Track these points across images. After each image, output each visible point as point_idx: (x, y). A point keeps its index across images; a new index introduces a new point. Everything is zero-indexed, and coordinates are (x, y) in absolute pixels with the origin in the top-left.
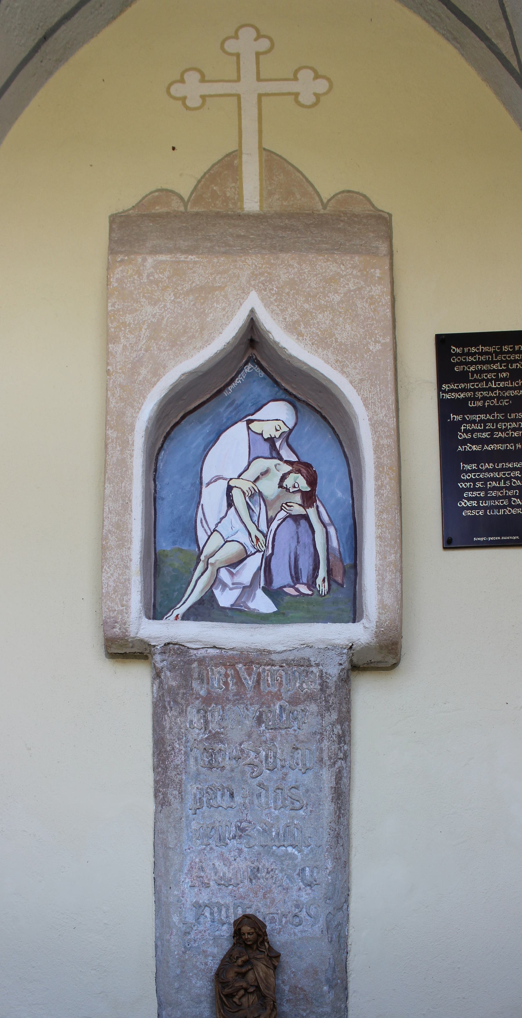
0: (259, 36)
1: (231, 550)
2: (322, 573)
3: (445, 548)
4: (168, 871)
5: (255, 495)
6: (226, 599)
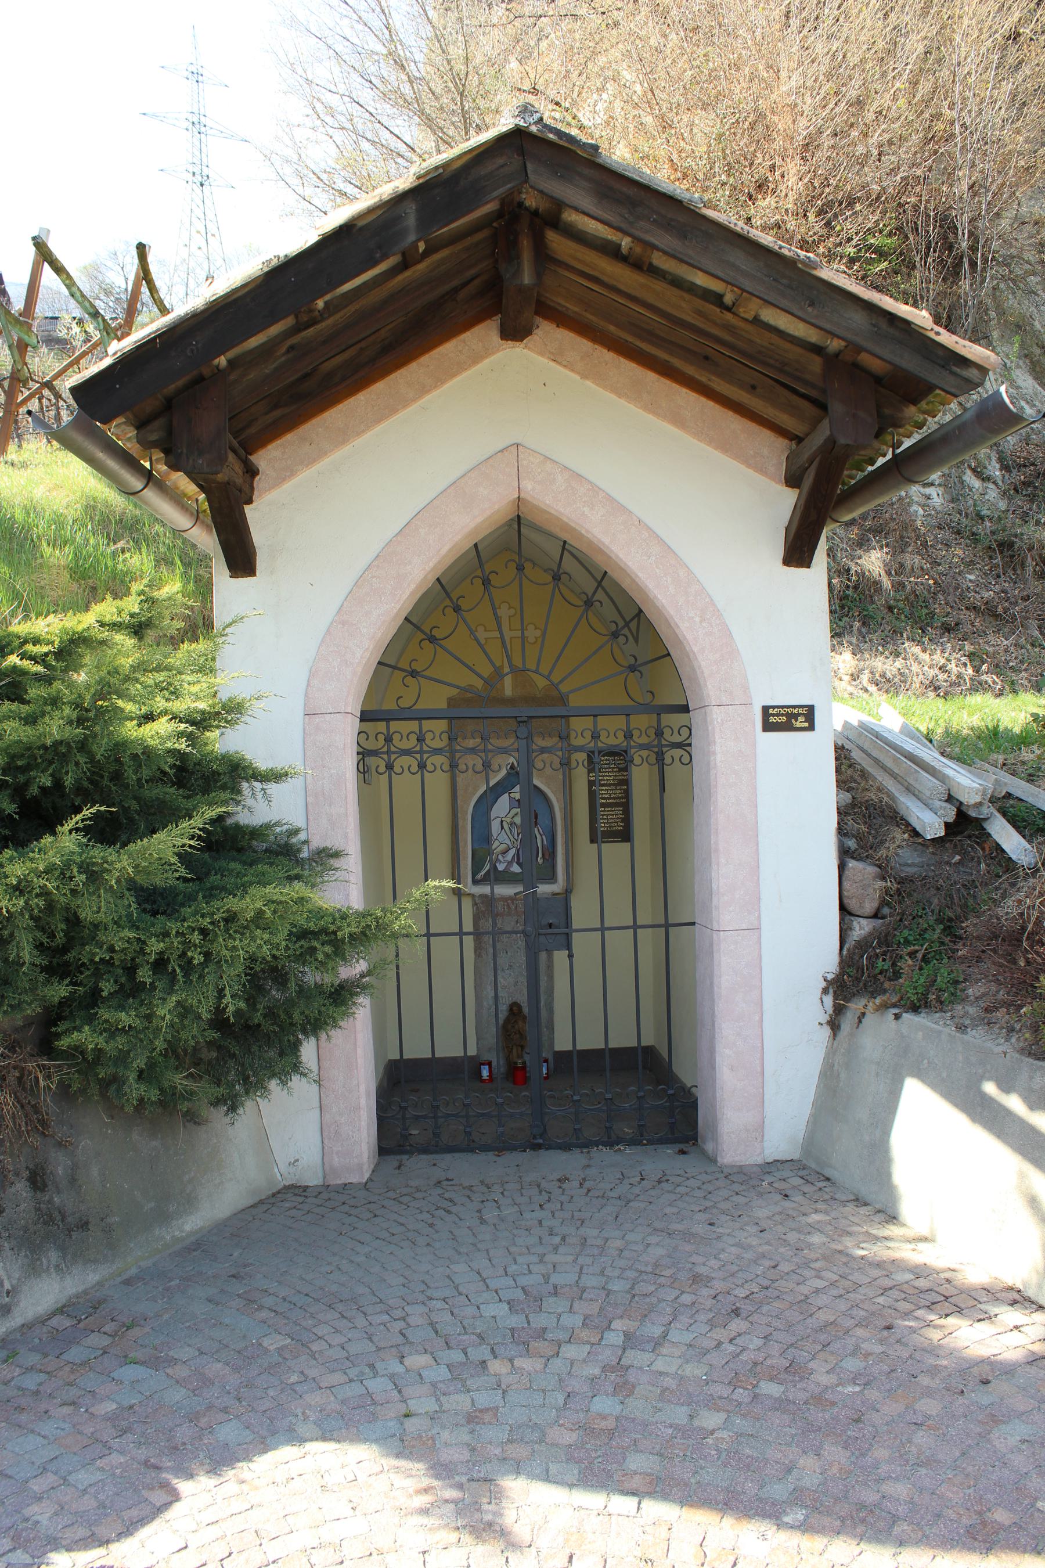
0: (510, 608)
1: (503, 846)
2: (540, 855)
3: (809, 567)
4: (40, 1499)
5: (513, 824)
6: (501, 867)
